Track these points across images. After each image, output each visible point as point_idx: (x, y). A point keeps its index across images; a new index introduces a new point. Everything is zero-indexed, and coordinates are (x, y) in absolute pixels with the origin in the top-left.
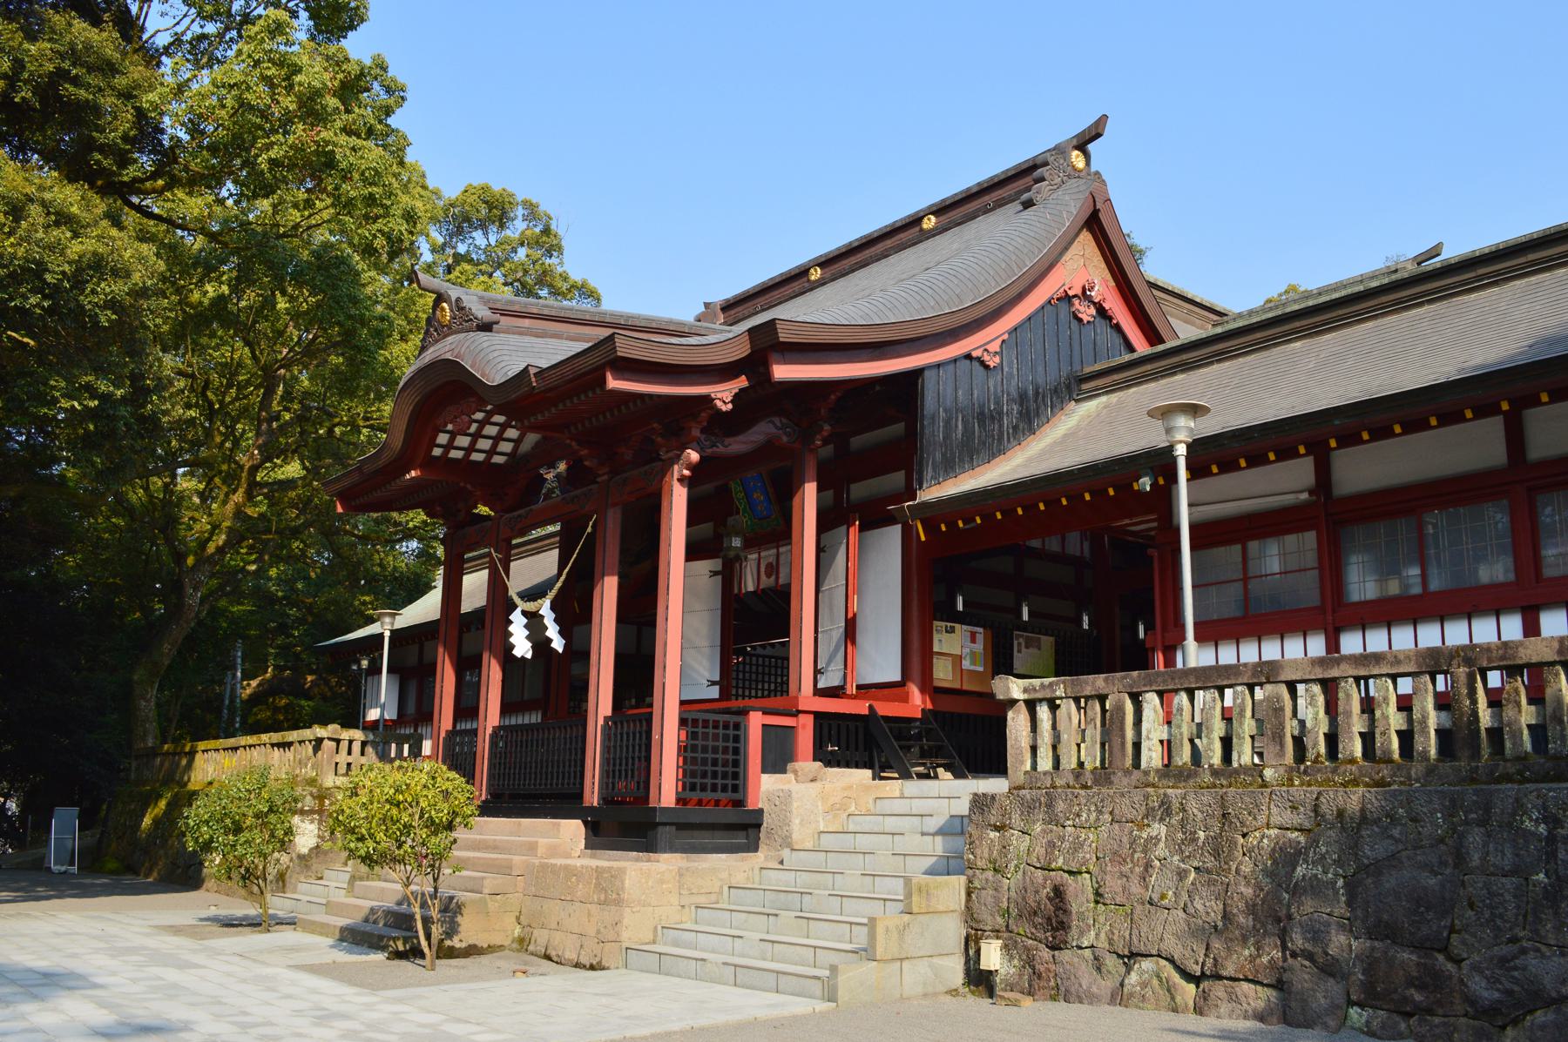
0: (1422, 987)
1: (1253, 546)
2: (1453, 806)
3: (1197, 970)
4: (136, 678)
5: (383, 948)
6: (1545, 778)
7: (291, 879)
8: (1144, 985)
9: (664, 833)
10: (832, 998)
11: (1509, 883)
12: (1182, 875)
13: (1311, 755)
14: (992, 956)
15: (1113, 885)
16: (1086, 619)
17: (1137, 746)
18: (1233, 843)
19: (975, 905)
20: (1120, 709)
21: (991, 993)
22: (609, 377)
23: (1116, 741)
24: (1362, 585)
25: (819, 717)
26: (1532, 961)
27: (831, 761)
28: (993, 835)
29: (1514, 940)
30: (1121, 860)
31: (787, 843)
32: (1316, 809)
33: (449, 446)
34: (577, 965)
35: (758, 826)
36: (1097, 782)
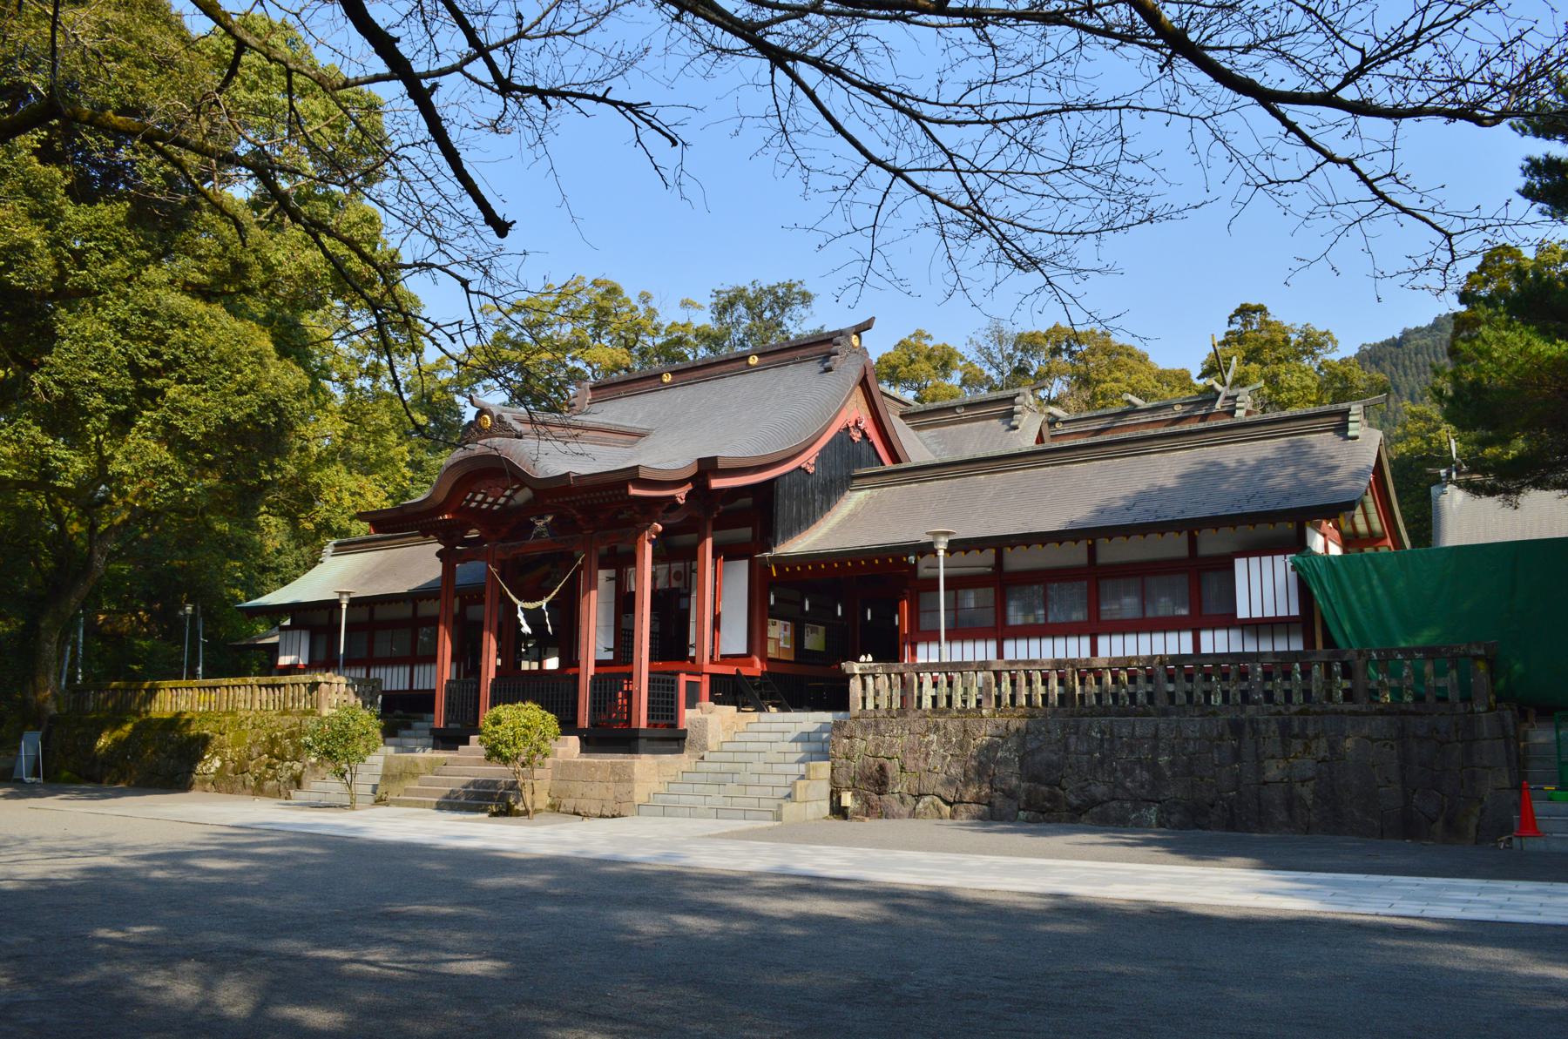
0: (1049, 801)
1: (961, 592)
2: (1064, 727)
3: (952, 800)
4: (43, 625)
5: (483, 811)
6: (1100, 715)
7: (306, 780)
8: (926, 808)
9: (642, 743)
10: (778, 818)
11: (1085, 757)
12: (944, 758)
13: (1003, 704)
14: (847, 799)
15: (910, 764)
16: (807, 603)
17: (920, 699)
18: (969, 743)
19: (836, 775)
20: (912, 680)
21: (845, 817)
22: (630, 487)
23: (909, 695)
24: (1015, 617)
25: (712, 676)
26: (1093, 788)
27: (718, 701)
28: (845, 741)
29: (1086, 780)
30: (912, 750)
31: (704, 747)
32: (1007, 728)
33: (472, 500)
34: (601, 816)
35: (684, 739)
36: (899, 715)
